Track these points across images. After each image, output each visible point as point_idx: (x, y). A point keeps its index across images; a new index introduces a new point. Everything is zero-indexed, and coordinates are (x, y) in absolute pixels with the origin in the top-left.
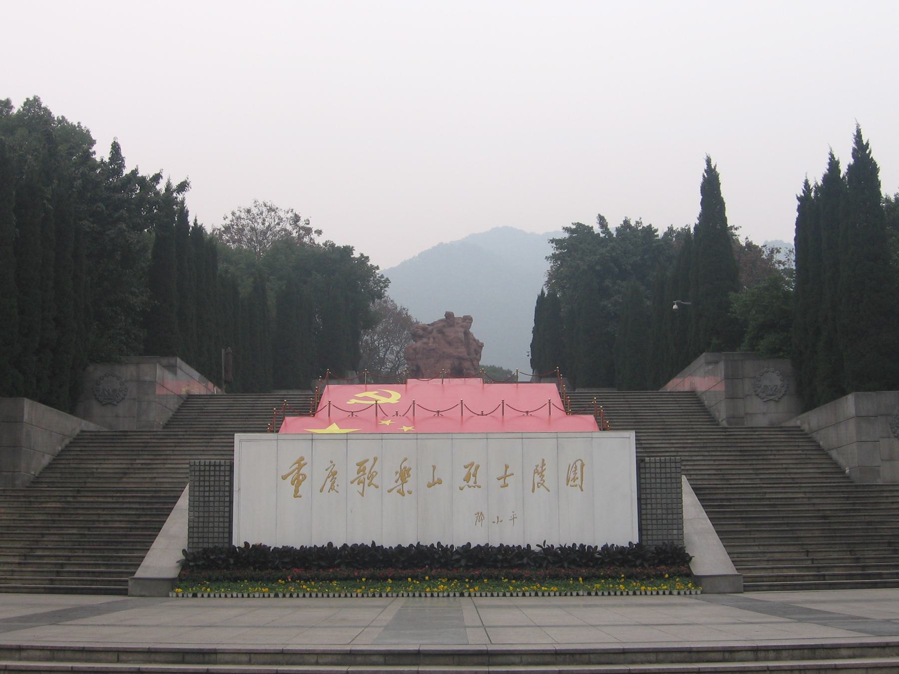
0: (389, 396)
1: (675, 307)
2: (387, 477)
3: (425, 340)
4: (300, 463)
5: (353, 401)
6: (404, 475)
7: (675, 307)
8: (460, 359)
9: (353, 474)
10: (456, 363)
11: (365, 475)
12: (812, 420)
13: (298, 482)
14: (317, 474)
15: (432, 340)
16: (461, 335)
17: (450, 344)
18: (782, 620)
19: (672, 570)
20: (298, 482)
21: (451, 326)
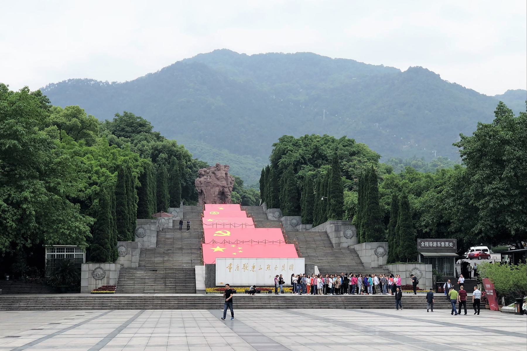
0: (226, 233)
1: (322, 199)
2: (250, 268)
3: (205, 177)
4: (231, 264)
5: (215, 235)
6: (254, 267)
7: (322, 199)
8: (224, 187)
9: (242, 267)
10: (221, 189)
11: (245, 267)
12: (357, 247)
13: (230, 269)
14: (234, 267)
15: (209, 177)
16: (224, 175)
17: (218, 179)
18: (405, 333)
19: (113, 187)
20: (230, 269)
21: (219, 170)
